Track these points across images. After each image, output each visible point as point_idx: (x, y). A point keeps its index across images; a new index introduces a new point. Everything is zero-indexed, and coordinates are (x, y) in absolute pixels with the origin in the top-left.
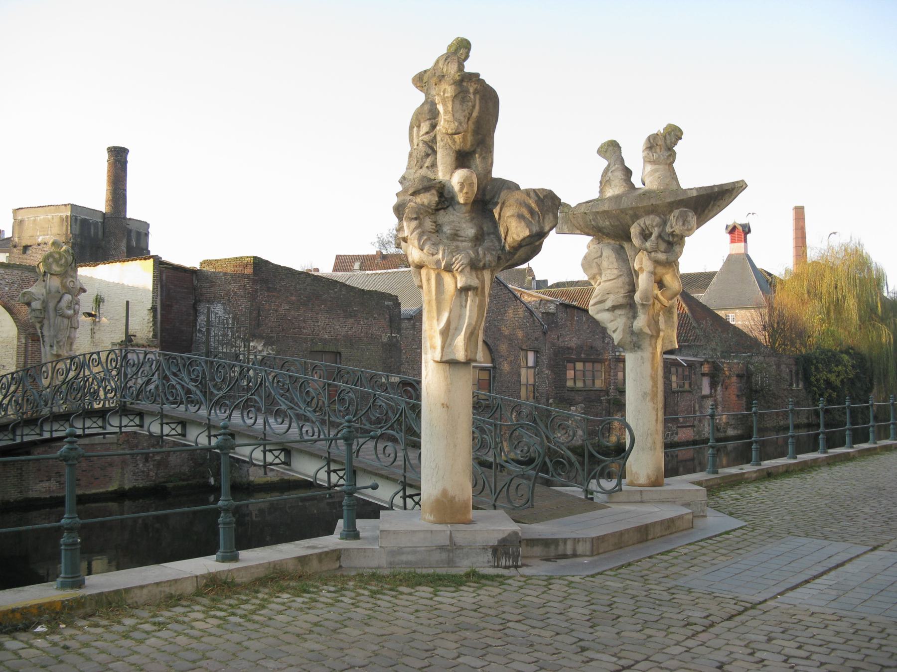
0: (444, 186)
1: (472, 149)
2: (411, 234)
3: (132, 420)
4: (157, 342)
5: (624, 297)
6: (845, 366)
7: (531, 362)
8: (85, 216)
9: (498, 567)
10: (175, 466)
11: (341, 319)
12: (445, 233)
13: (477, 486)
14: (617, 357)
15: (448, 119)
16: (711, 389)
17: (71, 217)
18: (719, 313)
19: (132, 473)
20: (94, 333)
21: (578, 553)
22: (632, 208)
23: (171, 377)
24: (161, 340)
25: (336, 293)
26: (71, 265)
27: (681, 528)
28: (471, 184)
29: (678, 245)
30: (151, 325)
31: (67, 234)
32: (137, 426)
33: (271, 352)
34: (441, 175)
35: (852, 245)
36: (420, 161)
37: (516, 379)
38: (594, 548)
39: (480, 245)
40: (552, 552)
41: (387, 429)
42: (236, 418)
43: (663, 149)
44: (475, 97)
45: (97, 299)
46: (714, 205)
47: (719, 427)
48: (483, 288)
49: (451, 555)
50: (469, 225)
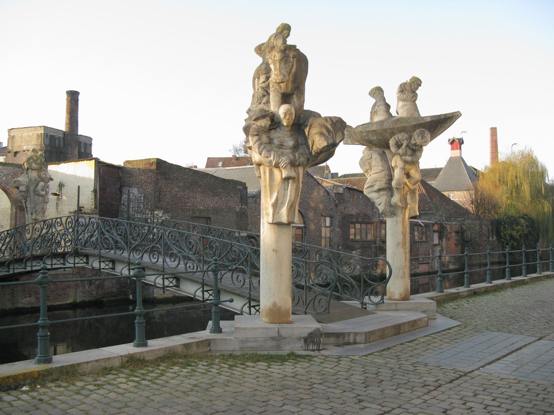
0: (274, 115)
1: (292, 92)
2: (254, 145)
3: (81, 260)
4: (97, 211)
5: (385, 183)
6: (522, 226)
7: (328, 224)
8: (52, 133)
9: (307, 350)
10: (108, 288)
11: (211, 197)
12: (275, 144)
13: (295, 300)
14: (381, 221)
15: (277, 74)
16: (439, 240)
17: (44, 134)
18: (444, 193)
19: (81, 292)
20: (58, 206)
21: (357, 342)
22: (390, 129)
23: (106, 233)
24: (99, 210)
25: (207, 181)
26: (44, 164)
27: (421, 326)
28: (291, 114)
29: (419, 151)
30: (93, 200)
31: (41, 144)
32: (85, 263)
33: (167, 217)
34: (272, 108)
35: (526, 152)
36: (259, 100)
37: (319, 234)
38: (367, 338)
39: (296, 151)
40: (341, 341)
41: (239, 265)
42: (146, 258)
43: (409, 92)
44: (293, 60)
45: (60, 184)
46: (441, 127)
47: (444, 264)
48: (298, 178)
49: (279, 342)
50: (290, 139)
